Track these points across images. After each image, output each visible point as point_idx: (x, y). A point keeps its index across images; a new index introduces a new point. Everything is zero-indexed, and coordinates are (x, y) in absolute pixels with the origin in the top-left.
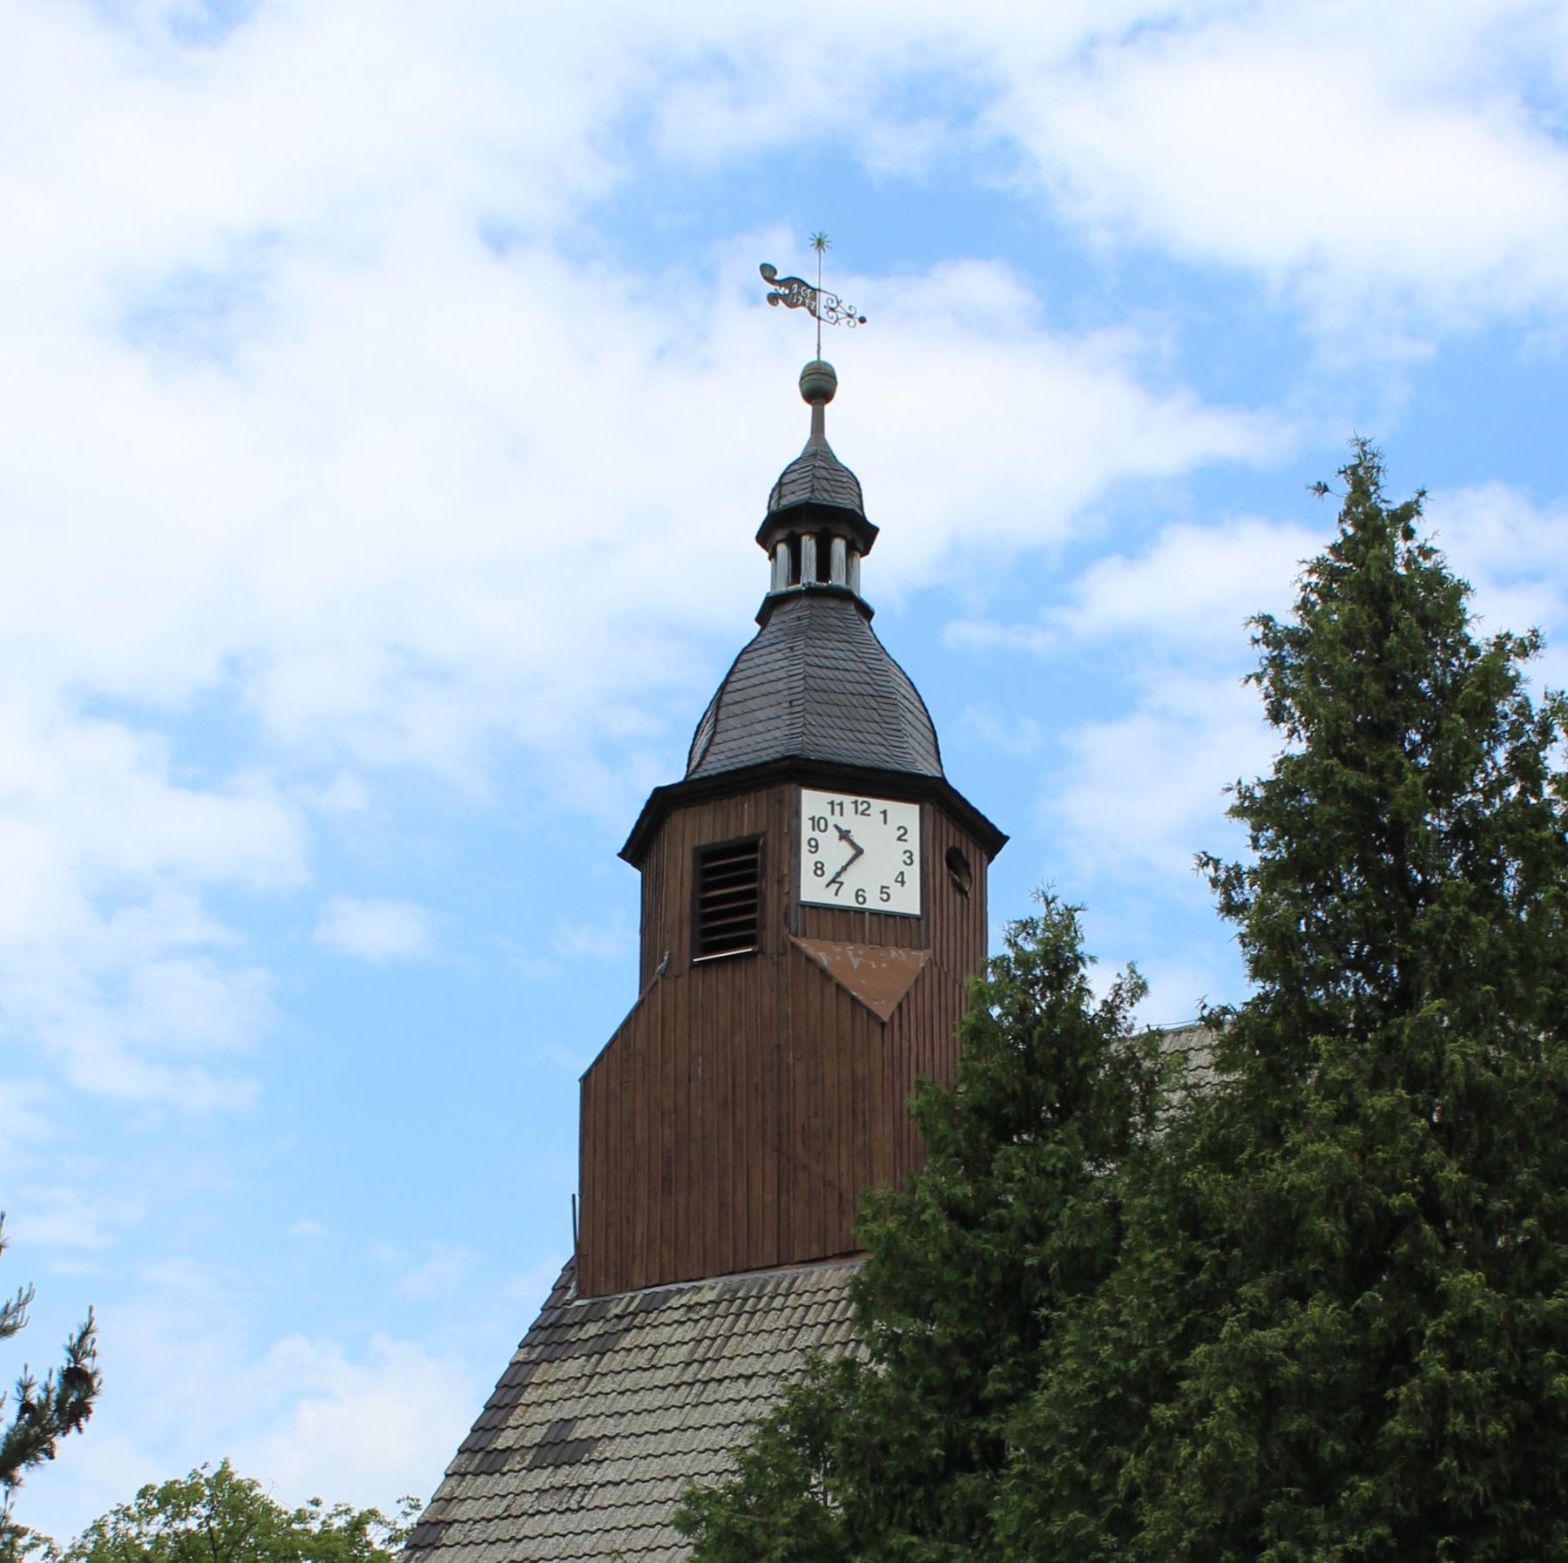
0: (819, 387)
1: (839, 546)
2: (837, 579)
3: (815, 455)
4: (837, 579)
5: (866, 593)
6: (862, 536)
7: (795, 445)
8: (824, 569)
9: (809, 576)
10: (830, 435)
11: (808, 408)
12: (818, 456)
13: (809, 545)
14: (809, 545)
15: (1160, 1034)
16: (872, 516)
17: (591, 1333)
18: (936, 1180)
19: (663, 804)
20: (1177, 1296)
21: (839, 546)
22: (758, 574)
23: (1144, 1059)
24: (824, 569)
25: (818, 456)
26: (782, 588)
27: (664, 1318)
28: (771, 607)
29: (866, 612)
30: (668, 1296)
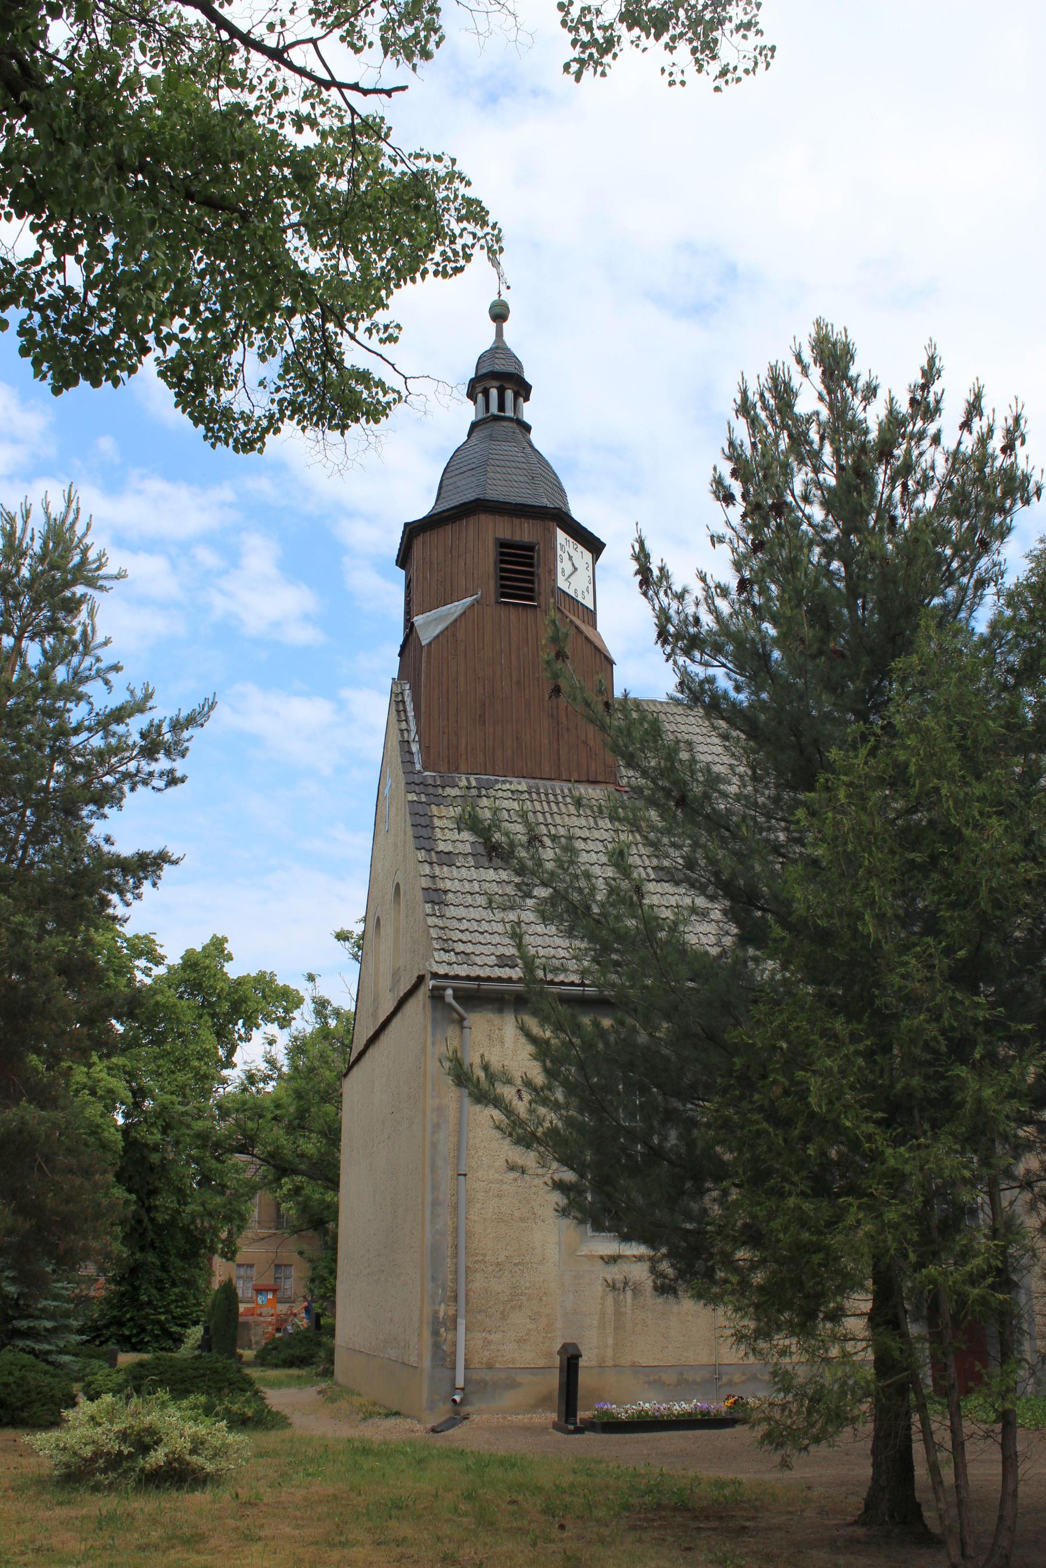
0: (499, 314)
1: (509, 394)
2: (509, 413)
3: (497, 348)
4: (509, 413)
5: (527, 418)
6: (523, 390)
7: (488, 342)
8: (501, 407)
9: (494, 409)
10: (506, 338)
11: (493, 326)
12: (499, 349)
13: (494, 393)
14: (494, 393)
15: (333, 1336)
16: (528, 377)
17: (948, 1435)
18: (811, 1448)
19: (413, 531)
20: (46, 820)
21: (509, 394)
22: (468, 412)
23: (843, 1350)
24: (501, 407)
25: (499, 349)
26: (480, 417)
27: (394, 809)
28: (474, 426)
29: (528, 428)
30: (497, 782)
